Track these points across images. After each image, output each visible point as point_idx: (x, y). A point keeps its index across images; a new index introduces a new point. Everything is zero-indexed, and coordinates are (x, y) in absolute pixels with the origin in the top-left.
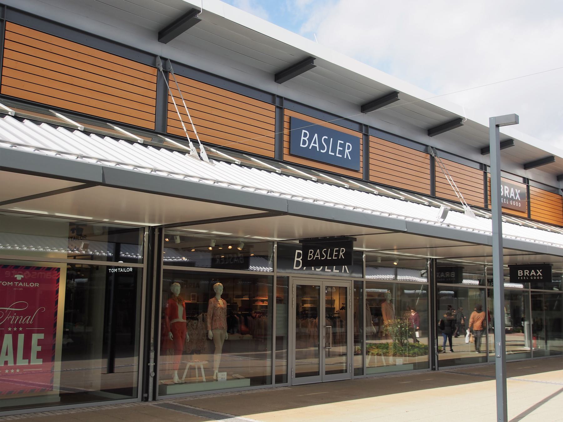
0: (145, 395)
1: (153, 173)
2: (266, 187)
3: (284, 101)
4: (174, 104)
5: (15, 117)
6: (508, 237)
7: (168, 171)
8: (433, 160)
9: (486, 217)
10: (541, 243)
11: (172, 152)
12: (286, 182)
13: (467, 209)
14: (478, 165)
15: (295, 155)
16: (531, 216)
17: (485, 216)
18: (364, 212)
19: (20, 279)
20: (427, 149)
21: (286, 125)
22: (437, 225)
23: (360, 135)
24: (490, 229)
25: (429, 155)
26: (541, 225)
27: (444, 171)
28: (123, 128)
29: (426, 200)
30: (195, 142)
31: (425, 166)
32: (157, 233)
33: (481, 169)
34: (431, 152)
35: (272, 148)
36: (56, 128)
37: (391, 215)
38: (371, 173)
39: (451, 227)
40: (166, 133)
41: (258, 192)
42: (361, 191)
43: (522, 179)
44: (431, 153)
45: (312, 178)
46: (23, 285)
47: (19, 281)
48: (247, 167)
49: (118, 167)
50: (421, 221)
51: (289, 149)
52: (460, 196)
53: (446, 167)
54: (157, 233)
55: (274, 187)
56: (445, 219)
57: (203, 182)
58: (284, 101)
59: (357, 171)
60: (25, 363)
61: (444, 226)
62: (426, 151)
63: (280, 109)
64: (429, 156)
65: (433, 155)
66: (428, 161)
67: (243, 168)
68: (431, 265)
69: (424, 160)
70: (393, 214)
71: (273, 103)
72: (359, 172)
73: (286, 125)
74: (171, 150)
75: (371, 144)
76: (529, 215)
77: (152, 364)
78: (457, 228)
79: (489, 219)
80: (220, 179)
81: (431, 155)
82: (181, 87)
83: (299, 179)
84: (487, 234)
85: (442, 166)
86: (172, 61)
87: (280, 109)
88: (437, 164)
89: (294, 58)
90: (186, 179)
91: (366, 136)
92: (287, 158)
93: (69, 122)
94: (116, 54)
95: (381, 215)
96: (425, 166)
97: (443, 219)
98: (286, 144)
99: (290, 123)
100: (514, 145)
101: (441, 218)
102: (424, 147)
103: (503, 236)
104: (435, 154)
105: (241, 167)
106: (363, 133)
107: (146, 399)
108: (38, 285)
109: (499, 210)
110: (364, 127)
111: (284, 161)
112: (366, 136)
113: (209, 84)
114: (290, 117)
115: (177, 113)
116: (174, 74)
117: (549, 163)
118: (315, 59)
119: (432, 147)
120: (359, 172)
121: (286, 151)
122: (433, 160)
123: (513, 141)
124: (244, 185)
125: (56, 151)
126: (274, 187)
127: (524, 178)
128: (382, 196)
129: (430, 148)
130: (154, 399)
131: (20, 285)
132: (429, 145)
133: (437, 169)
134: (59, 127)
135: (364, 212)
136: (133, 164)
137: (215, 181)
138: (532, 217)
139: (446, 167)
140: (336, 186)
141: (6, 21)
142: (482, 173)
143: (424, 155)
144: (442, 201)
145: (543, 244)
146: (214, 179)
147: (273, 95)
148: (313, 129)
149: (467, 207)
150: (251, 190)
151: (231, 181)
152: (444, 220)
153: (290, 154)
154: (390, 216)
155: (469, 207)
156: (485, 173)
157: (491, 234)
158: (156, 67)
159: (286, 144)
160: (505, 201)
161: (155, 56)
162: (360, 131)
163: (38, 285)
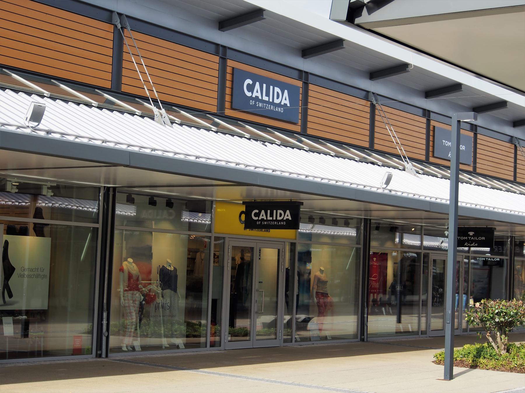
0: (99, 352)
1: (104, 144)
2: (185, 151)
3: (228, 50)
4: (136, 63)
5: (98, 107)
6: (464, 205)
7: (75, 135)
8: (373, 107)
9: (488, 187)
10: (482, 208)
11: (101, 110)
12: (256, 150)
13: (409, 165)
14: (213, 46)
15: (252, 113)
16: (517, 178)
17: (245, 135)
18: (282, 174)
19: (472, 235)
20: (512, 140)
21: (229, 77)
22: (380, 191)
23: (300, 84)
24: (448, 197)
25: (514, 145)
26: (496, 183)
27: (385, 120)
28: (356, 149)
29: (509, 185)
30: (405, 158)
31: (363, 114)
32: (111, 193)
33: (424, 115)
34: (516, 143)
35: (109, 76)
36: (4, 91)
37: (308, 177)
38: (309, 125)
39: (393, 193)
40: (224, 115)
41: (118, 147)
42: (467, 183)
43: (421, 111)
44: (516, 144)
45: (355, 158)
46: (474, 238)
47: (471, 236)
48: (197, 129)
49: (153, 154)
50: (414, 195)
51: (231, 102)
52: (401, 150)
53: (388, 115)
54: (111, 193)
55: (248, 160)
56: (388, 185)
57: (36, 134)
58: (228, 50)
59: (469, 165)
60: (271, 218)
61: (386, 192)
62: (366, 98)
63: (224, 59)
64: (513, 146)
65: (375, 102)
66: (368, 110)
67: (282, 147)
68: (511, 241)
69: (364, 106)
70: (340, 181)
71: (216, 54)
72: (297, 124)
73: (229, 77)
74: (122, 112)
75: (310, 93)
76: (475, 168)
77: (105, 322)
78: (398, 194)
79: (490, 188)
80: (109, 139)
81: (515, 146)
82: (136, 44)
83: (385, 167)
84: (444, 202)
85: (383, 115)
86: (128, 16)
87: (224, 59)
88: (377, 112)
89: (323, 39)
90: (129, 148)
91: (306, 84)
92: (228, 112)
93: (83, 98)
94: (86, 16)
95: (344, 185)
96: (363, 114)
97: (386, 185)
98: (228, 98)
99: (233, 74)
100: (344, 47)
101: (384, 184)
102: (364, 93)
103: (459, 204)
104: (376, 100)
105: (217, 133)
106: (303, 81)
107: (100, 356)
108: (484, 239)
109: (457, 167)
110: (221, 48)
111: (226, 115)
112: (306, 84)
113: (185, 45)
114: (233, 68)
115: (146, 74)
116: (131, 30)
117: (404, 73)
118: (462, 85)
119: (373, 93)
120: (297, 124)
121: (227, 105)
122: (373, 107)
123: (506, 103)
124: (217, 159)
125: (44, 130)
126: (248, 160)
127: (424, 110)
128: (494, 189)
129: (371, 95)
130: (107, 356)
131: (489, 260)
132: (370, 90)
133: (377, 118)
134: (58, 100)
135: (282, 174)
136: (88, 137)
137: (104, 141)
138: (478, 171)
139: (388, 115)
140: (387, 167)
141: (227, 59)
142: (424, 120)
143: (508, 145)
144: (325, 143)
145: (470, 206)
146: (151, 147)
147: (217, 45)
148: (255, 78)
149: (408, 163)
150: (98, 143)
151: (187, 152)
152: (38, 125)
153: (232, 108)
154: (337, 183)
155: (163, 111)
156: (429, 121)
157: (448, 202)
158: (113, 23)
159: (228, 98)
160: (269, 107)
161: (111, 12)
162: (300, 79)
163: (484, 239)
